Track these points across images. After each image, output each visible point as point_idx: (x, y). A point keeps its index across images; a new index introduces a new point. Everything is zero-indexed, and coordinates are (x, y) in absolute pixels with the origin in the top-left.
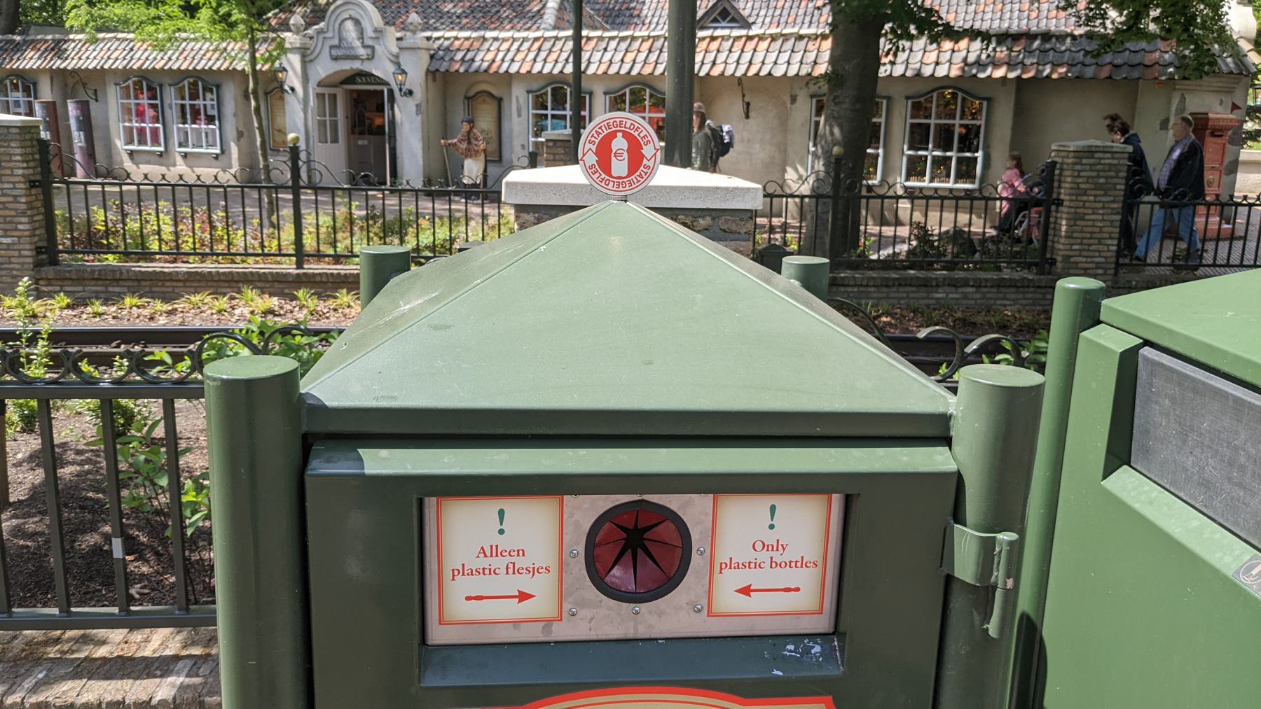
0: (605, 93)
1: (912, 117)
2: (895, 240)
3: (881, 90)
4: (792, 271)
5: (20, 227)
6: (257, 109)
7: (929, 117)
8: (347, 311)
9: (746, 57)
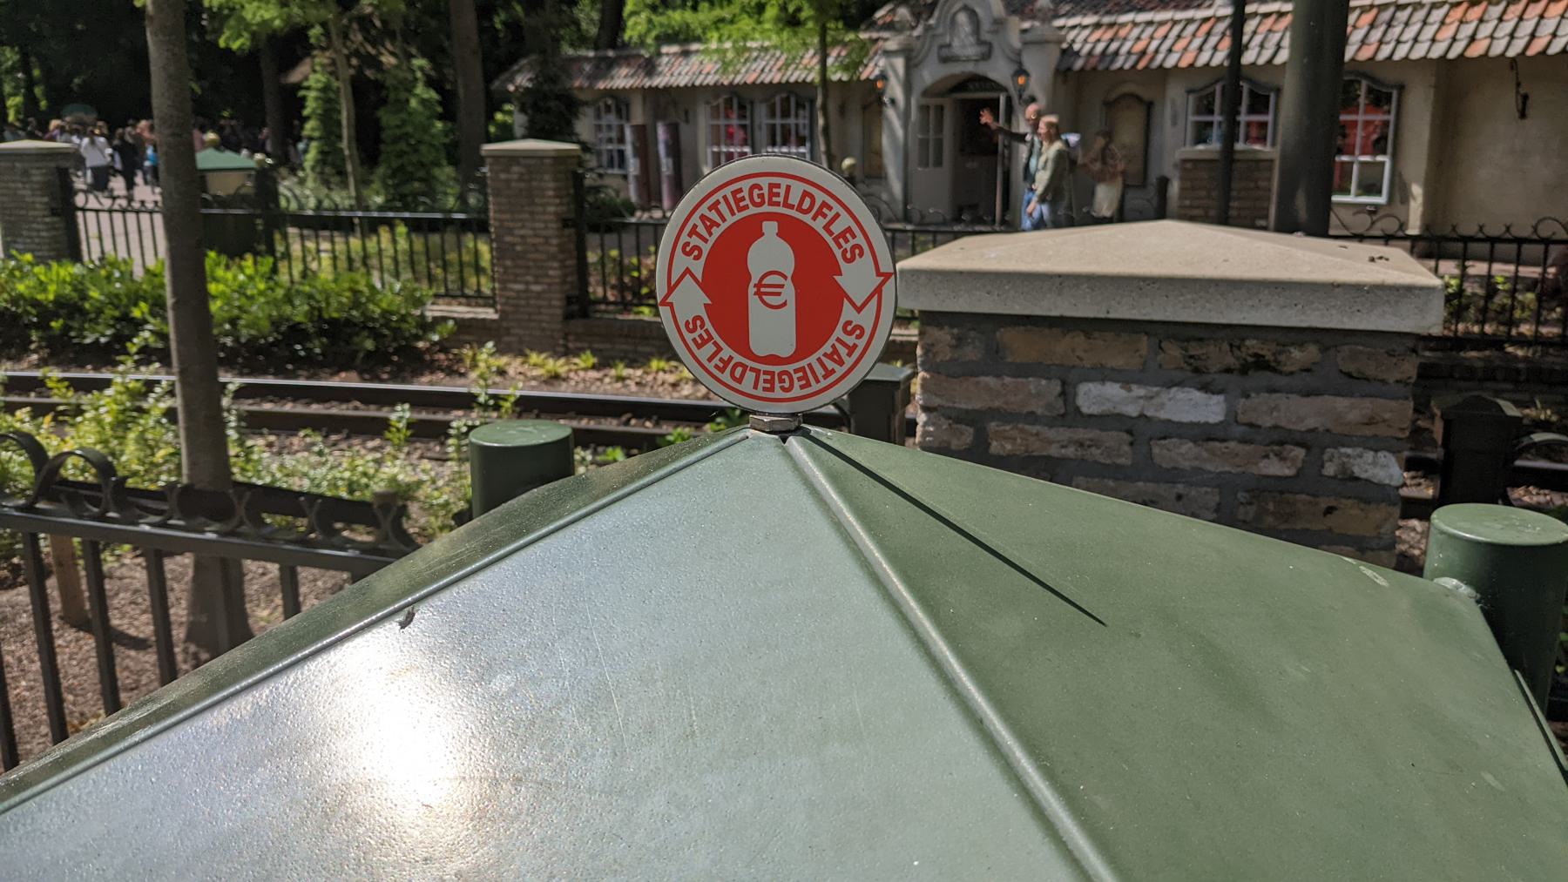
5: (551, 273)
6: (826, 130)
9: (1527, 27)
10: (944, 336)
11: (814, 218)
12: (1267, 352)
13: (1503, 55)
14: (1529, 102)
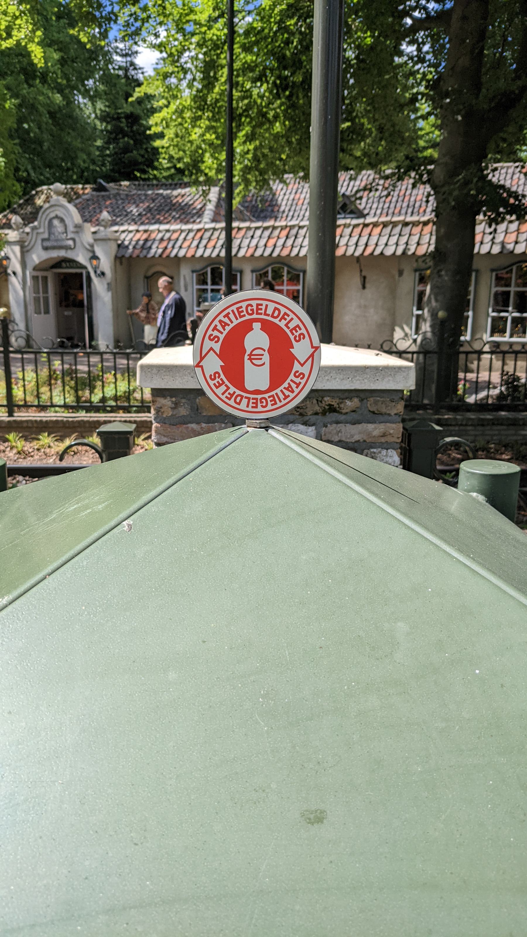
0: (253, 271)
1: (497, 285)
2: (488, 385)
3: (476, 264)
4: (475, 482)
7: (509, 285)
8: (48, 450)
9: (363, 240)
10: (166, 402)
11: (280, 321)
12: (334, 403)
13: (353, 255)
14: (367, 280)
